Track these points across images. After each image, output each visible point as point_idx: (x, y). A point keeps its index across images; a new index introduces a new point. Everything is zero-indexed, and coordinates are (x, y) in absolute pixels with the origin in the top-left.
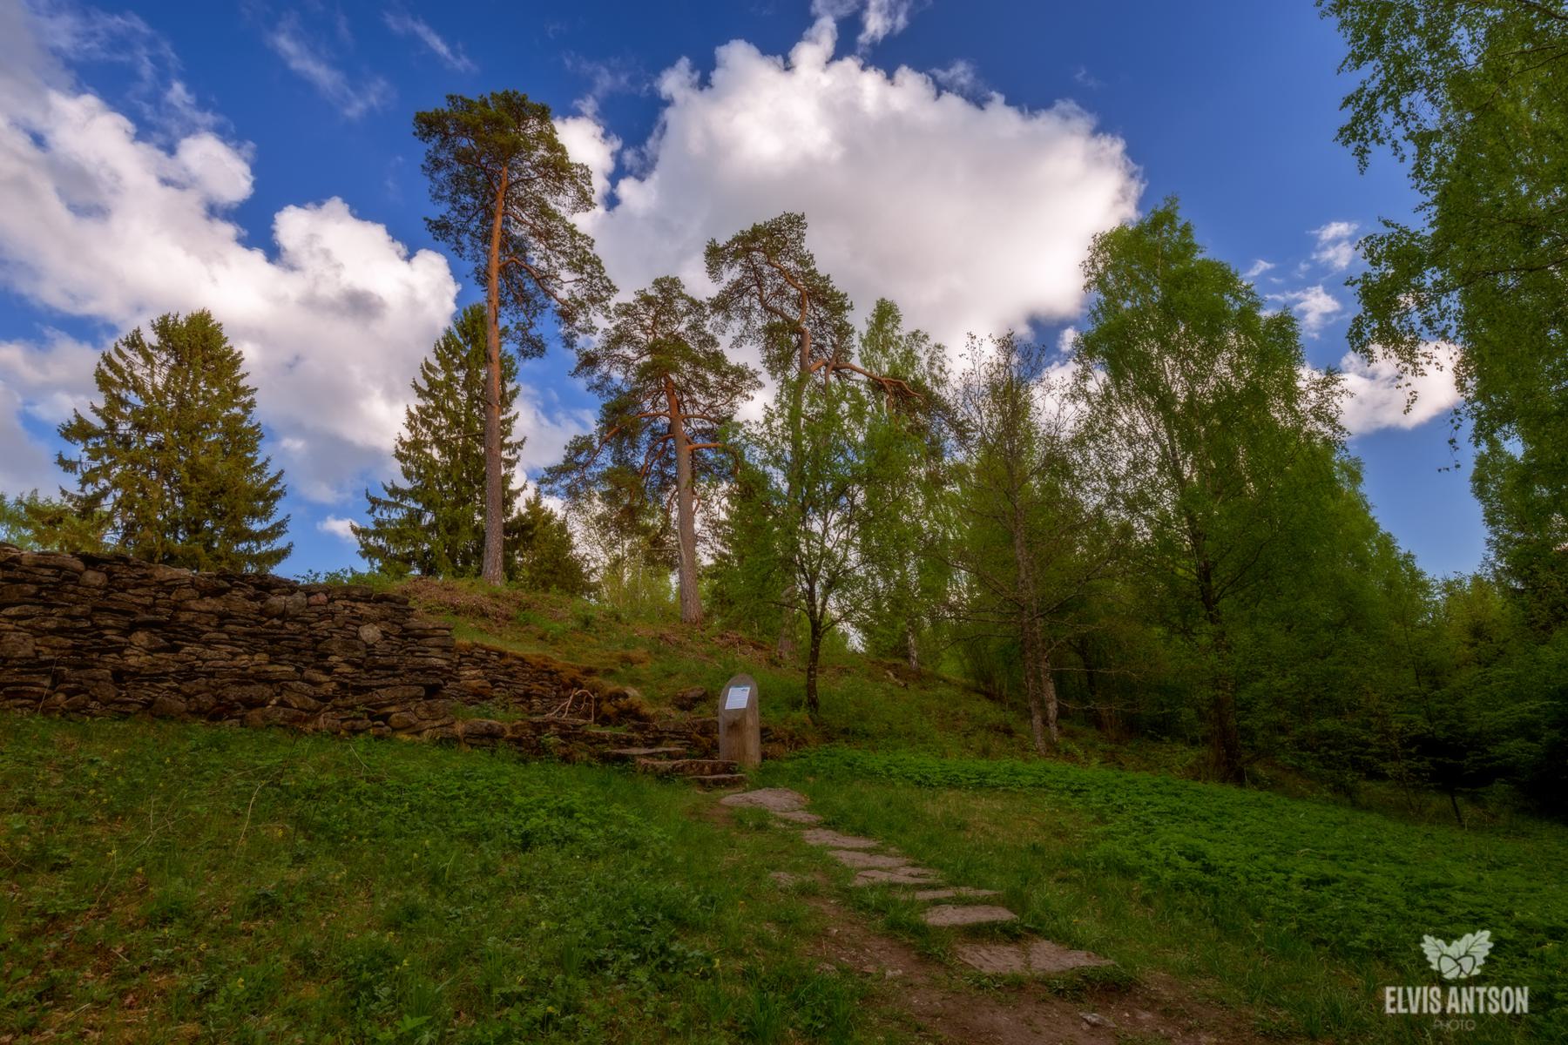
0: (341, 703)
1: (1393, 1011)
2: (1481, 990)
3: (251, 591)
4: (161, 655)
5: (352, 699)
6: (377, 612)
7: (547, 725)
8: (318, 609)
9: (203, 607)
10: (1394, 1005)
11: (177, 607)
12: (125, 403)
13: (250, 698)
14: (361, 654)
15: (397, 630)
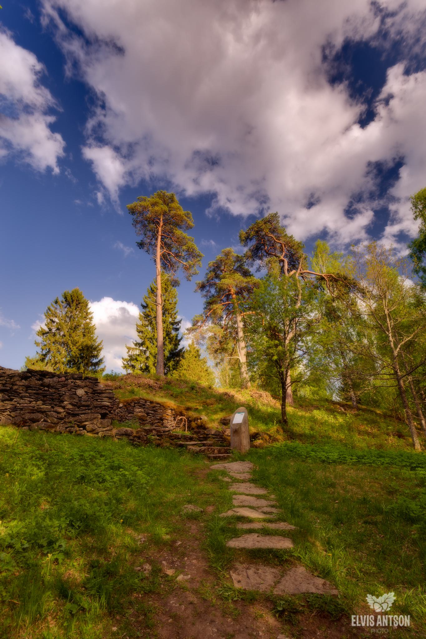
0: (67, 420)
1: (355, 625)
2: (391, 617)
3: (38, 377)
4: (6, 402)
5: (71, 419)
6: (84, 384)
7: (150, 431)
8: (61, 383)
9: (21, 384)
10: (355, 623)
11: (13, 384)
12: (53, 322)
13: (33, 418)
14: (76, 400)
15: (91, 390)
